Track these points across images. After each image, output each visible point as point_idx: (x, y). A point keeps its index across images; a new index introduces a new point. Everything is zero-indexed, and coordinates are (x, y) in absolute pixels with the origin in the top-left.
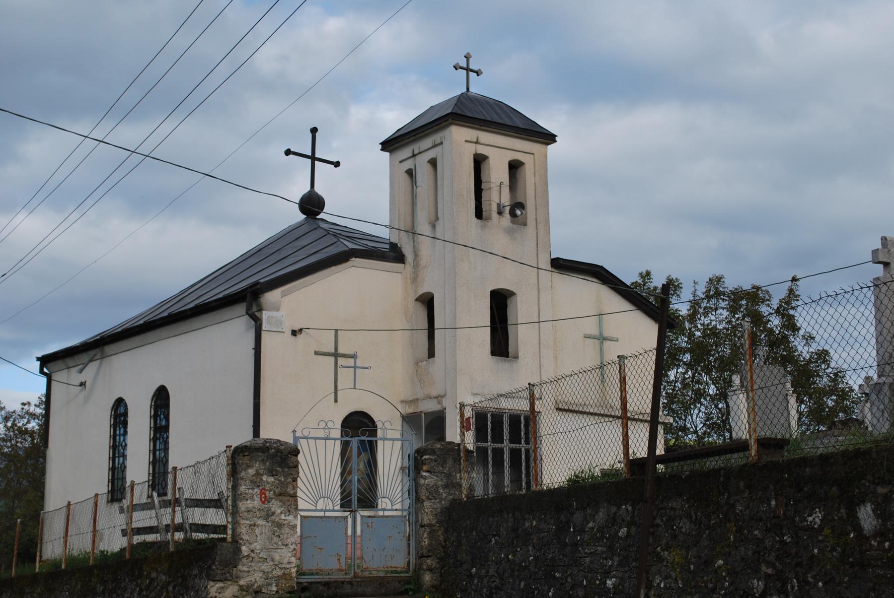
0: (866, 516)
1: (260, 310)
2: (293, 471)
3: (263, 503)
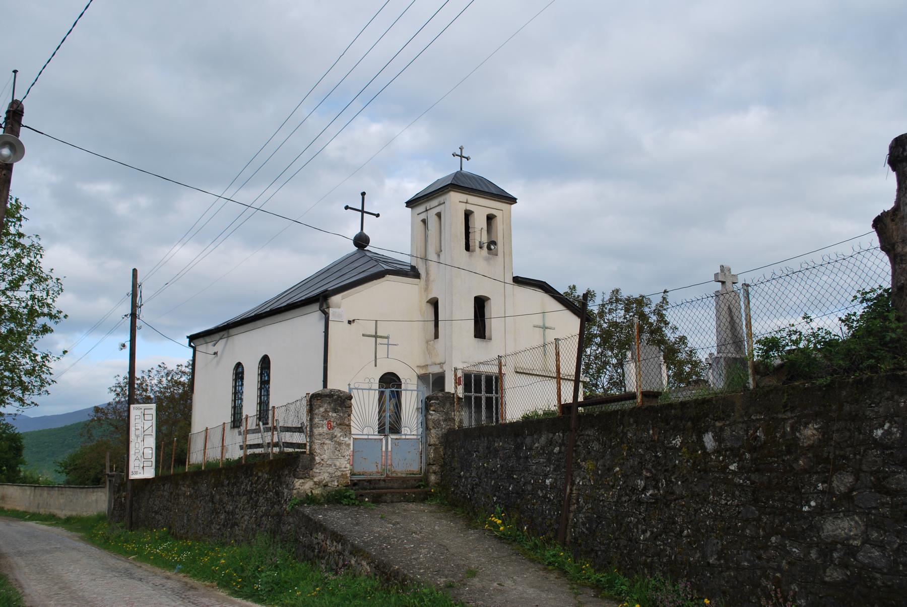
0: (709, 440)
1: (328, 307)
2: (348, 410)
3: (329, 429)
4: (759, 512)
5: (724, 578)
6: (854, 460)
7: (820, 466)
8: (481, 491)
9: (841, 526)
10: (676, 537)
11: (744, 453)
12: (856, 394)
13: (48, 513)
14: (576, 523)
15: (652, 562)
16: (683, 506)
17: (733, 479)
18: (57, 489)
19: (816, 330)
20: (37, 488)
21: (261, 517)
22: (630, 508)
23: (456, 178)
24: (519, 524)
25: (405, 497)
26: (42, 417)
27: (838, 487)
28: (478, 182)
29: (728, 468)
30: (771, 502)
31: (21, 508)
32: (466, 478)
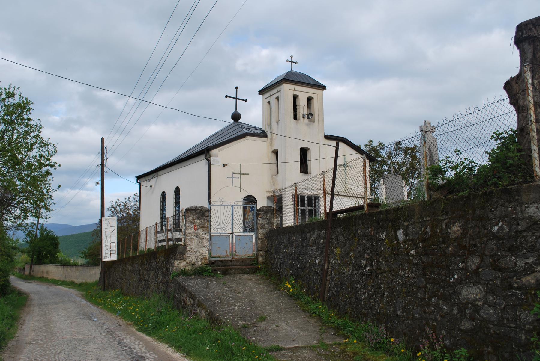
0: (400, 234)
1: (210, 157)
2: (207, 218)
3: (195, 230)
4: (426, 282)
5: (405, 325)
6: (481, 247)
7: (461, 251)
8: (285, 267)
9: (472, 292)
10: (380, 297)
11: (419, 243)
12: (483, 202)
13: (70, 281)
14: (330, 288)
15: (368, 313)
16: (385, 277)
17: (412, 260)
18: (74, 267)
19: (463, 160)
20: (65, 267)
21: (160, 283)
22: (358, 278)
23: (287, 76)
24: (302, 287)
25: (243, 271)
26: (80, 226)
27: (471, 265)
28: (301, 77)
29: (410, 253)
30: (433, 275)
31: (57, 278)
32: (278, 259)
